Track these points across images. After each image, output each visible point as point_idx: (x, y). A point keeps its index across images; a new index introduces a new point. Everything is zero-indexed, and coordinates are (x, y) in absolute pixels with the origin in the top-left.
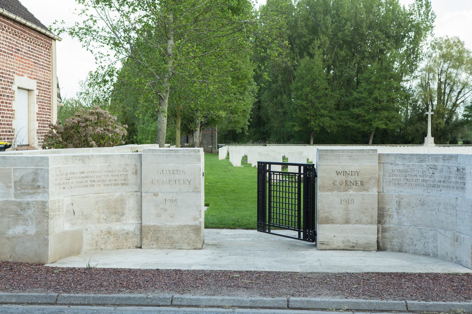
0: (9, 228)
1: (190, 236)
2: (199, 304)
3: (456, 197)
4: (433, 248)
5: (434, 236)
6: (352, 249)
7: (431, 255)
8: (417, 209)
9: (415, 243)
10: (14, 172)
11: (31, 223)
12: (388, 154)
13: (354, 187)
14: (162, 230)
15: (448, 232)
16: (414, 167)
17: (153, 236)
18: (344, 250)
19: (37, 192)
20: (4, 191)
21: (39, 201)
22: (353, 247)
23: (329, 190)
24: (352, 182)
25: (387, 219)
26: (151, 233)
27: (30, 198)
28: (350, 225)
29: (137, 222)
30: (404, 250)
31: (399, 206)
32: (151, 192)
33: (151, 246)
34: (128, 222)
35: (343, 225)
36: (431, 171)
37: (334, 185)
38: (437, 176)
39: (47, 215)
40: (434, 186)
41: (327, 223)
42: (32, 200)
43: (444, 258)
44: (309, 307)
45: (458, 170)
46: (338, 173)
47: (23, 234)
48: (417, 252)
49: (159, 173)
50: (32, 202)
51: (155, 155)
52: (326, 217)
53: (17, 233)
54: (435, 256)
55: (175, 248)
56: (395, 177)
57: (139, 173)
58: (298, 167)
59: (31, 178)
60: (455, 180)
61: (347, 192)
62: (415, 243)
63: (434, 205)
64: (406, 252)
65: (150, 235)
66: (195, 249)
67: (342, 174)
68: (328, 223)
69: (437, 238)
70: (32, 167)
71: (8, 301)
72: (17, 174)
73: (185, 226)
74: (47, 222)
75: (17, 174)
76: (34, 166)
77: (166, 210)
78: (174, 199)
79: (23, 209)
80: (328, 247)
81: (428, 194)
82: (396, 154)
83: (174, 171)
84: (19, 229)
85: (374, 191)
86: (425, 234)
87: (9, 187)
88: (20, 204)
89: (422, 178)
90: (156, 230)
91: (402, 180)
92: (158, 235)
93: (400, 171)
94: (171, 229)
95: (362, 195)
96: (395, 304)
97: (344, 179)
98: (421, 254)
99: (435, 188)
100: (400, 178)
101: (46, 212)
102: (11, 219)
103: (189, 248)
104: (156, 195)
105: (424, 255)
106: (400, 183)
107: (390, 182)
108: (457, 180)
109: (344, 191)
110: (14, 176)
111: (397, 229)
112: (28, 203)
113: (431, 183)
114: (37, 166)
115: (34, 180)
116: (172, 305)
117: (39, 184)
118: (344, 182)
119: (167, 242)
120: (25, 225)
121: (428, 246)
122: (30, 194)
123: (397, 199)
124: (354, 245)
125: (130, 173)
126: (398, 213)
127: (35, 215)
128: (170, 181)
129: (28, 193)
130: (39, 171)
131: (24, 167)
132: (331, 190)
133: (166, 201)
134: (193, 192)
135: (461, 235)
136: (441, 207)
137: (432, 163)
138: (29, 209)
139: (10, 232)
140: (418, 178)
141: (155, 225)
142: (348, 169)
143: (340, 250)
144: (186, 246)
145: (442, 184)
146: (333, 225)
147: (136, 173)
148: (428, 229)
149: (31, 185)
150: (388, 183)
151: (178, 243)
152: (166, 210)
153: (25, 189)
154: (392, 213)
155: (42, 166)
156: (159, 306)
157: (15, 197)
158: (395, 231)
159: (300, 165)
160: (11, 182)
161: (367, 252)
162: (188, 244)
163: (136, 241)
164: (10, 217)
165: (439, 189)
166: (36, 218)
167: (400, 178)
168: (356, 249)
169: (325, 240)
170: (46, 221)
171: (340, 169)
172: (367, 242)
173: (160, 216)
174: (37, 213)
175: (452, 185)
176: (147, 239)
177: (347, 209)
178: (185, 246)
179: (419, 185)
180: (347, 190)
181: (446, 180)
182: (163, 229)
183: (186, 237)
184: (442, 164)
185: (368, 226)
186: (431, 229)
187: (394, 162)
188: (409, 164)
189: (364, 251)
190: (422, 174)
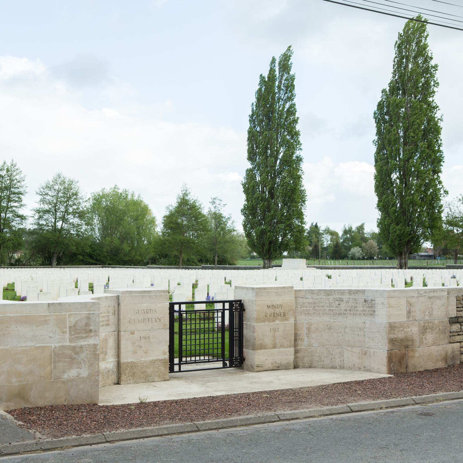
0: (64, 372)
1: (160, 369)
2: (297, 416)
3: (364, 321)
4: (340, 362)
5: (340, 353)
6: (278, 368)
7: (338, 367)
8: (325, 333)
9: (323, 359)
10: (69, 317)
11: (84, 366)
12: (300, 290)
13: (279, 317)
14: (138, 366)
15: (355, 348)
16: (321, 300)
17: (130, 372)
18: (272, 370)
19: (89, 336)
20: (60, 337)
21: (91, 344)
22: (278, 367)
23: (263, 321)
24: (278, 314)
25: (299, 342)
26: (129, 369)
27: (83, 342)
28: (277, 349)
29: (114, 360)
30: (314, 366)
31: (309, 331)
32: (129, 331)
33: (129, 381)
34: (109, 361)
35: (272, 350)
36: (337, 303)
37: (266, 317)
38: (343, 306)
39: (98, 357)
40: (340, 314)
41: (261, 349)
42: (85, 344)
43: (352, 368)
44: (293, 417)
45: (365, 301)
46: (268, 307)
47: (76, 377)
48: (325, 366)
49: (135, 313)
50: (85, 345)
51: (132, 296)
52: (261, 344)
53: (71, 377)
54: (342, 367)
55: (148, 381)
56: (306, 309)
57: (116, 313)
58: (222, 304)
59: (84, 322)
60: (362, 309)
61: (275, 322)
62: (323, 359)
63: (340, 328)
64: (315, 367)
65: (128, 371)
66: (164, 381)
67: (271, 307)
68: (262, 349)
69: (343, 354)
70: (85, 312)
71: (225, 426)
72: (72, 319)
73: (157, 360)
74: (98, 364)
75: (72, 319)
76: (87, 311)
77: (141, 347)
78: (147, 336)
79: (77, 353)
80: (262, 369)
81: (334, 321)
82: (306, 290)
83: (147, 310)
84: (73, 373)
85: (292, 321)
86: (332, 352)
87: (64, 332)
88: (74, 348)
89: (329, 309)
90: (133, 365)
91: (311, 310)
92: (134, 370)
93: (309, 303)
94: (145, 364)
95: (284, 323)
96: (407, 400)
97: (272, 311)
98: (328, 368)
99: (341, 316)
100: (310, 308)
101: (97, 354)
102: (66, 364)
103: (159, 380)
104: (132, 333)
105: (331, 368)
106: (310, 312)
107: (301, 312)
108: (365, 309)
109: (272, 322)
110: (69, 321)
111: (308, 350)
112: (81, 347)
113: (338, 312)
114: (90, 311)
115: (87, 325)
116: (280, 420)
117: (91, 328)
118: (273, 314)
119: (142, 377)
120: (79, 368)
121: (335, 361)
122: (83, 338)
123: (307, 326)
124: (279, 365)
125: (111, 314)
126: (308, 337)
127: (87, 358)
128: (144, 319)
129: (81, 337)
130: (91, 316)
131: (78, 313)
132: (264, 321)
133: (141, 338)
134: (163, 328)
135: (371, 349)
136: (347, 330)
137: (337, 296)
138: (82, 352)
139: (65, 376)
140: (325, 308)
141: (131, 362)
142: (275, 303)
143: (270, 370)
144: (157, 378)
145: (348, 312)
146: (265, 350)
147: (115, 314)
148: (335, 347)
149: (84, 330)
150: (299, 313)
151: (151, 376)
152: (141, 347)
153: (78, 333)
154: (303, 338)
155: (94, 311)
156: (274, 422)
157: (70, 341)
158: (306, 352)
159: (224, 302)
160: (66, 328)
161: (288, 370)
162: (159, 376)
163: (114, 378)
164: (65, 362)
165: (345, 316)
166: (89, 361)
167: (310, 308)
168: (280, 368)
169: (260, 363)
170: (97, 362)
171: (269, 303)
172: (287, 362)
173: (136, 353)
174: (89, 356)
175: (358, 312)
176: (125, 375)
177: (274, 337)
178: (157, 379)
179: (326, 314)
180: (274, 321)
181: (352, 309)
182: (139, 365)
183: (157, 370)
184: (348, 297)
185: (288, 349)
186: (337, 347)
187: (304, 296)
188: (317, 297)
189: (285, 369)
190: (329, 305)
